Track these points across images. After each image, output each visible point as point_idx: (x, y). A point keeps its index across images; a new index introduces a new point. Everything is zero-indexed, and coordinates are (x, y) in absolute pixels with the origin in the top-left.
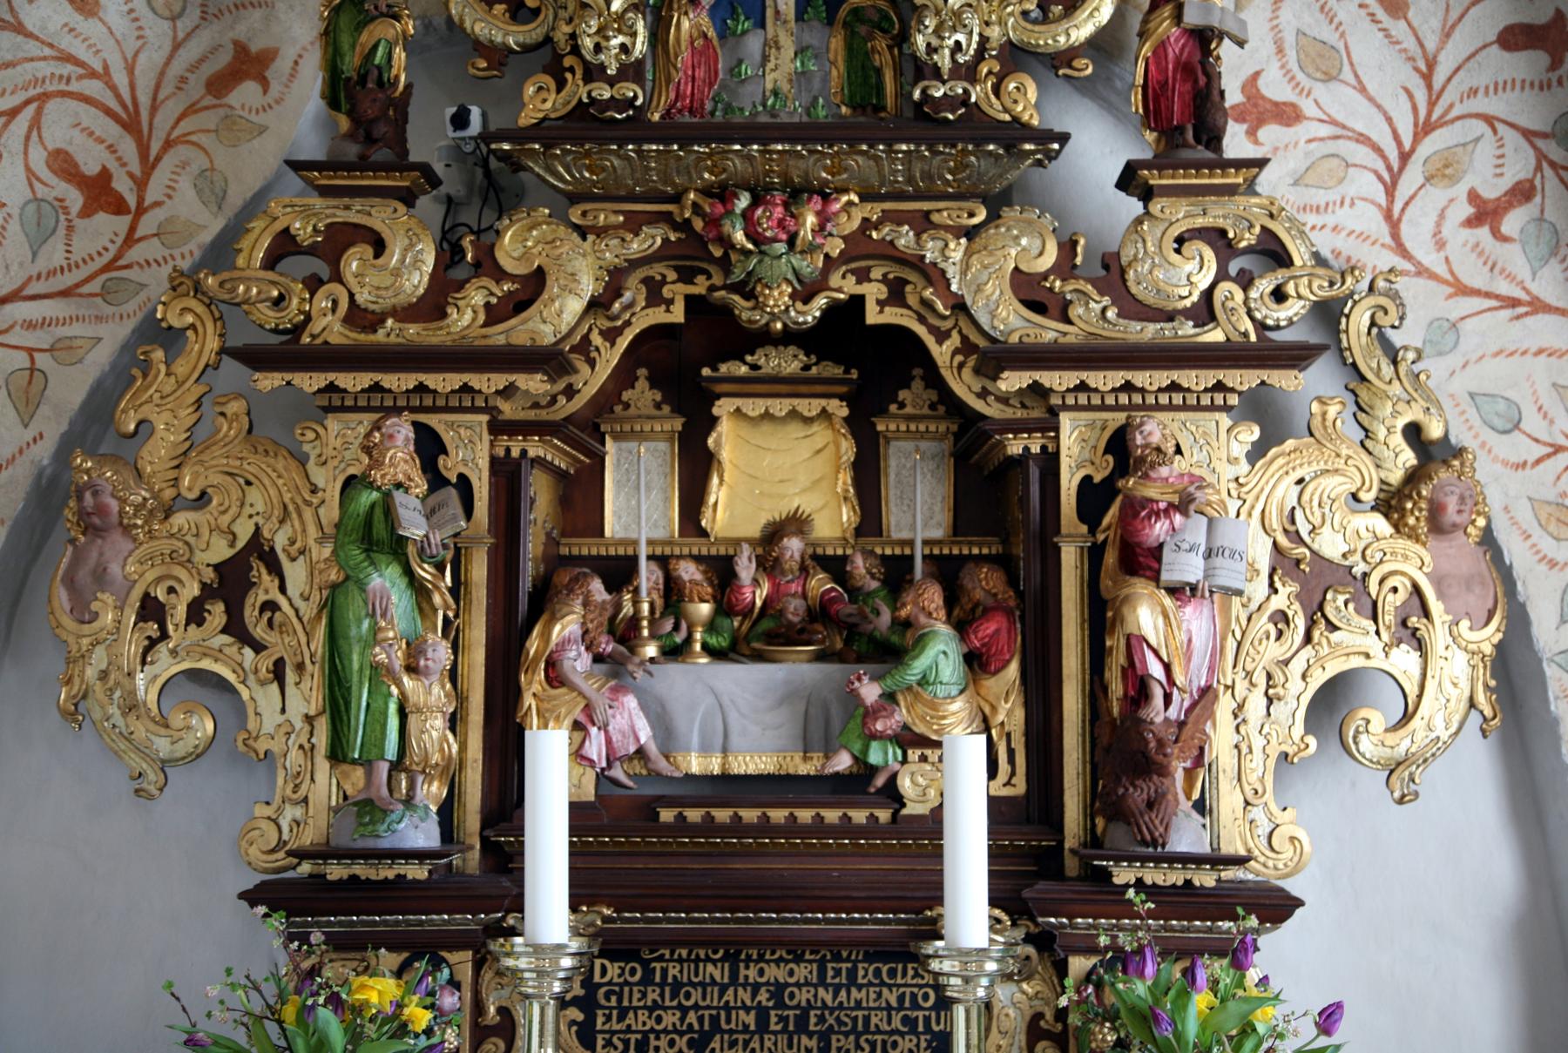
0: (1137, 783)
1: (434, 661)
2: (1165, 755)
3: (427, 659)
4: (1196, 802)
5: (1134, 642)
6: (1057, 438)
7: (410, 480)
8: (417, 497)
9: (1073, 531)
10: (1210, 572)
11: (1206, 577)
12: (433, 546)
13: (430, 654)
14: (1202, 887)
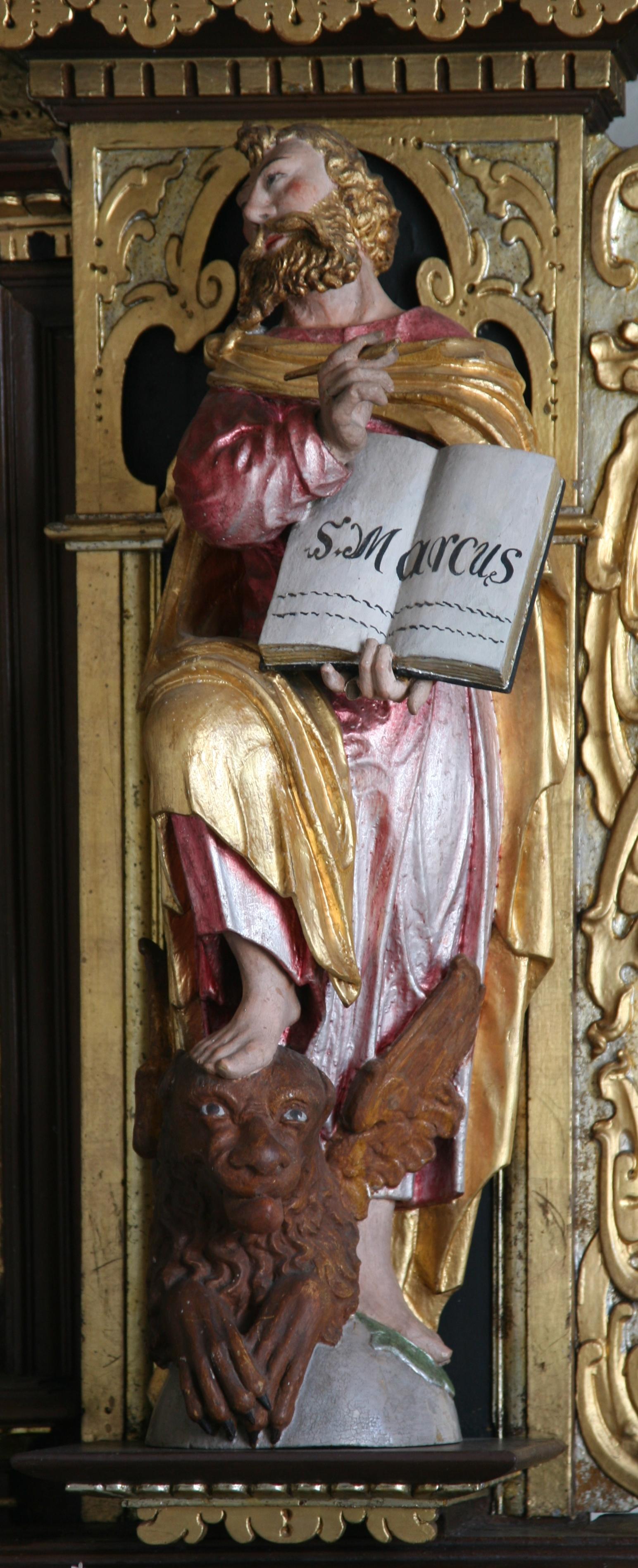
0: (220, 1250)
2: (255, 1170)
4: (457, 1297)
5: (183, 835)
6: (65, 207)
9: (111, 505)
10: (409, 618)
11: (392, 636)
14: (396, 1544)
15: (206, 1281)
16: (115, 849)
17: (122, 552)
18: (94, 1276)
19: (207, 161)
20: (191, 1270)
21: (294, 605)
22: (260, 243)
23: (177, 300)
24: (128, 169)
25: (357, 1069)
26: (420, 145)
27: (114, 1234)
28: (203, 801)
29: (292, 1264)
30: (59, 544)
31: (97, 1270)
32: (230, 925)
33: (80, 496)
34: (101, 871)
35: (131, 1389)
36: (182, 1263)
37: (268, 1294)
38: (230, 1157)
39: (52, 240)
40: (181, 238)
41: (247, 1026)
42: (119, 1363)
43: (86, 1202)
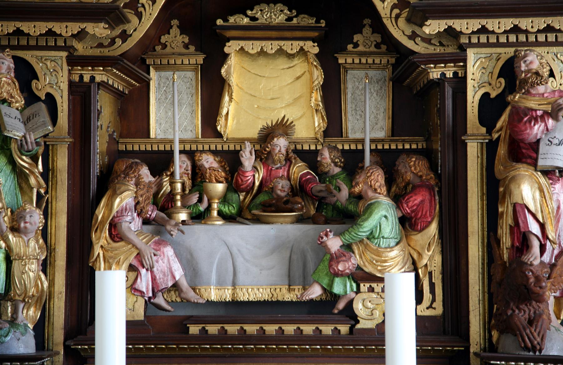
1: (31, 224)
2: (541, 287)
3: (26, 223)
5: (518, 208)
7: (12, 97)
8: (17, 109)
9: (475, 132)
12: (29, 144)
13: (28, 219)
15: (518, 314)
16: (477, 211)
17: (478, 142)
18: (473, 312)
19: (498, 56)
20: (514, 311)
21: (546, 156)
22: (523, 75)
23: (491, 87)
24: (480, 58)
25: (550, 264)
26: (548, 53)
27: (477, 302)
28: (527, 200)
29: (538, 311)
30: (464, 140)
31: (473, 310)
32: (530, 229)
33: (468, 130)
34: (473, 216)
35: (481, 340)
36: (512, 309)
37: (534, 318)
38: (534, 284)
39: (458, 73)
40: (492, 73)
41: (534, 253)
42: (479, 333)
43: (470, 294)
